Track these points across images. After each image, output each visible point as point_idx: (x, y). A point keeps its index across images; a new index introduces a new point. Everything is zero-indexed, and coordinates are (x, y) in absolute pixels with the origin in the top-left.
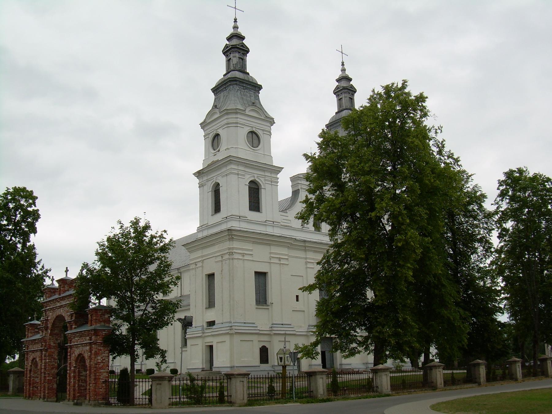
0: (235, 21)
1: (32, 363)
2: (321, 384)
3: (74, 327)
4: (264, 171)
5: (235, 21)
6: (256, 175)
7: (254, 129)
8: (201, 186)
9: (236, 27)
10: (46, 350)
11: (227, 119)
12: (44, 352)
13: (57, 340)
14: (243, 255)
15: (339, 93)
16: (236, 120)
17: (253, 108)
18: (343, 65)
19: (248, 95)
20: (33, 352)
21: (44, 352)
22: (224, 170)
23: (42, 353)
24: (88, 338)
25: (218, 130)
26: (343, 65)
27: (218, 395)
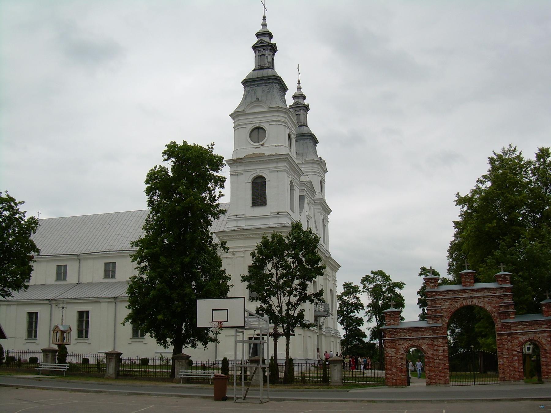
0: (264, 18)
2: (111, 370)
5: (264, 18)
7: (257, 125)
9: (264, 25)
11: (277, 116)
15: (298, 109)
16: (276, 117)
18: (299, 83)
22: (272, 165)
26: (299, 83)
27: (322, 375)
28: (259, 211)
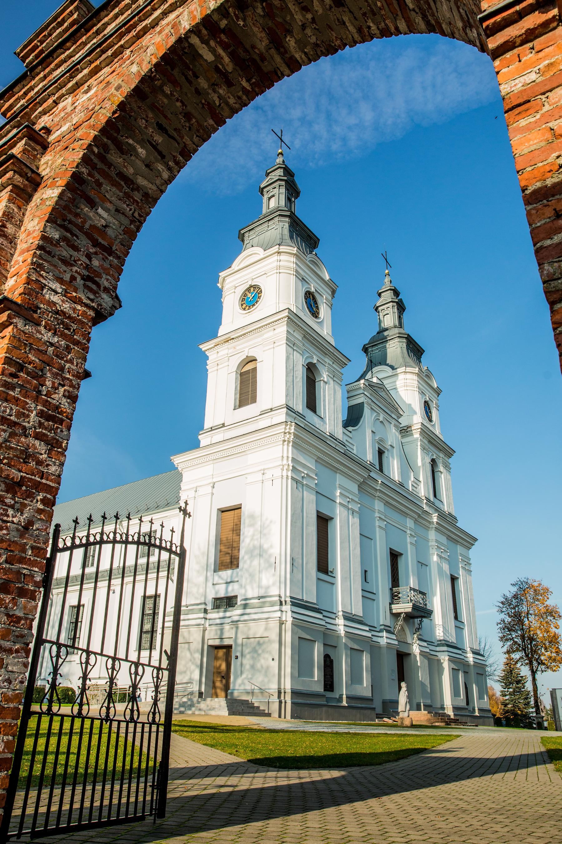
28: (249, 410)
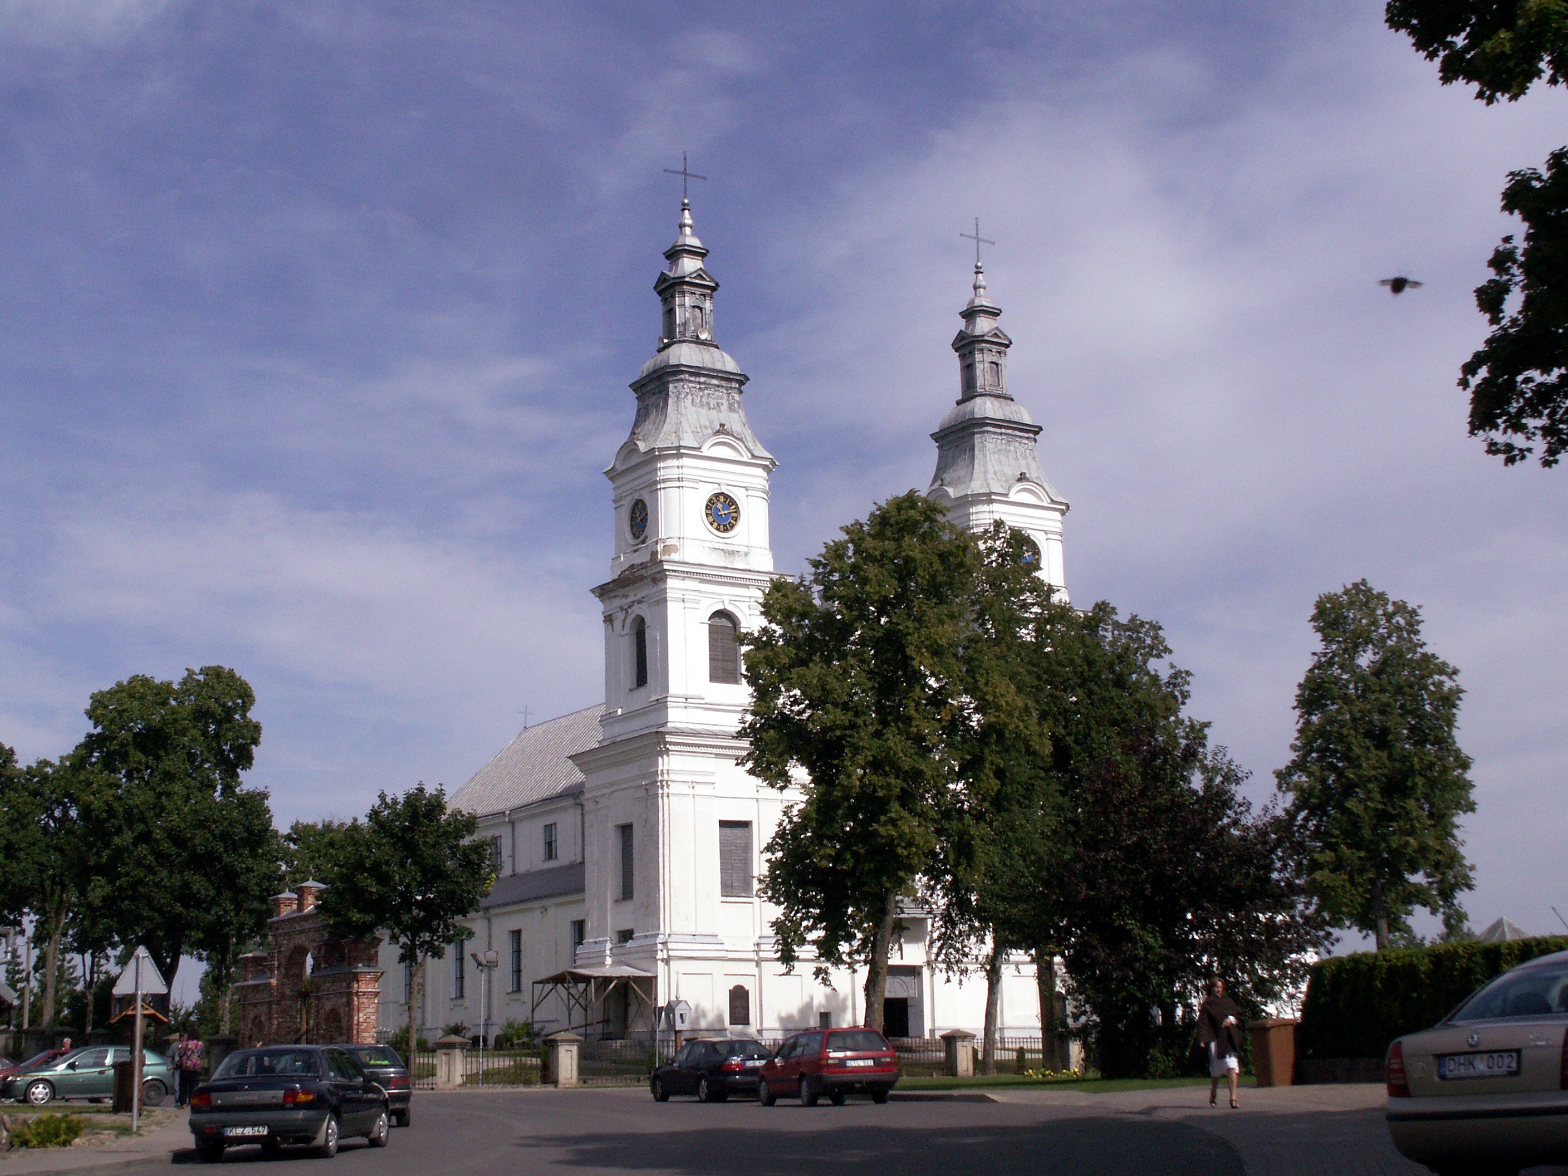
1: (253, 1024)
3: (323, 966)
4: (747, 586)
6: (726, 599)
8: (609, 619)
10: (278, 1003)
12: (274, 1006)
13: (295, 984)
14: (693, 784)
17: (722, 438)
19: (713, 403)
20: (255, 1005)
21: (274, 1006)
23: (270, 1008)
24: (344, 984)
25: (642, 492)
